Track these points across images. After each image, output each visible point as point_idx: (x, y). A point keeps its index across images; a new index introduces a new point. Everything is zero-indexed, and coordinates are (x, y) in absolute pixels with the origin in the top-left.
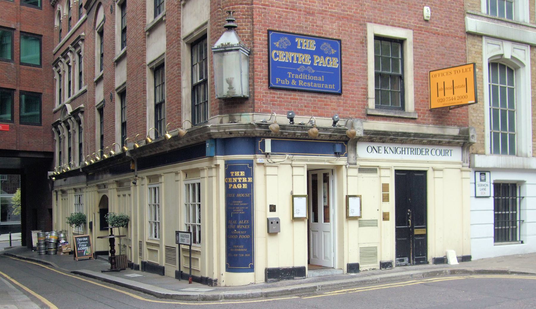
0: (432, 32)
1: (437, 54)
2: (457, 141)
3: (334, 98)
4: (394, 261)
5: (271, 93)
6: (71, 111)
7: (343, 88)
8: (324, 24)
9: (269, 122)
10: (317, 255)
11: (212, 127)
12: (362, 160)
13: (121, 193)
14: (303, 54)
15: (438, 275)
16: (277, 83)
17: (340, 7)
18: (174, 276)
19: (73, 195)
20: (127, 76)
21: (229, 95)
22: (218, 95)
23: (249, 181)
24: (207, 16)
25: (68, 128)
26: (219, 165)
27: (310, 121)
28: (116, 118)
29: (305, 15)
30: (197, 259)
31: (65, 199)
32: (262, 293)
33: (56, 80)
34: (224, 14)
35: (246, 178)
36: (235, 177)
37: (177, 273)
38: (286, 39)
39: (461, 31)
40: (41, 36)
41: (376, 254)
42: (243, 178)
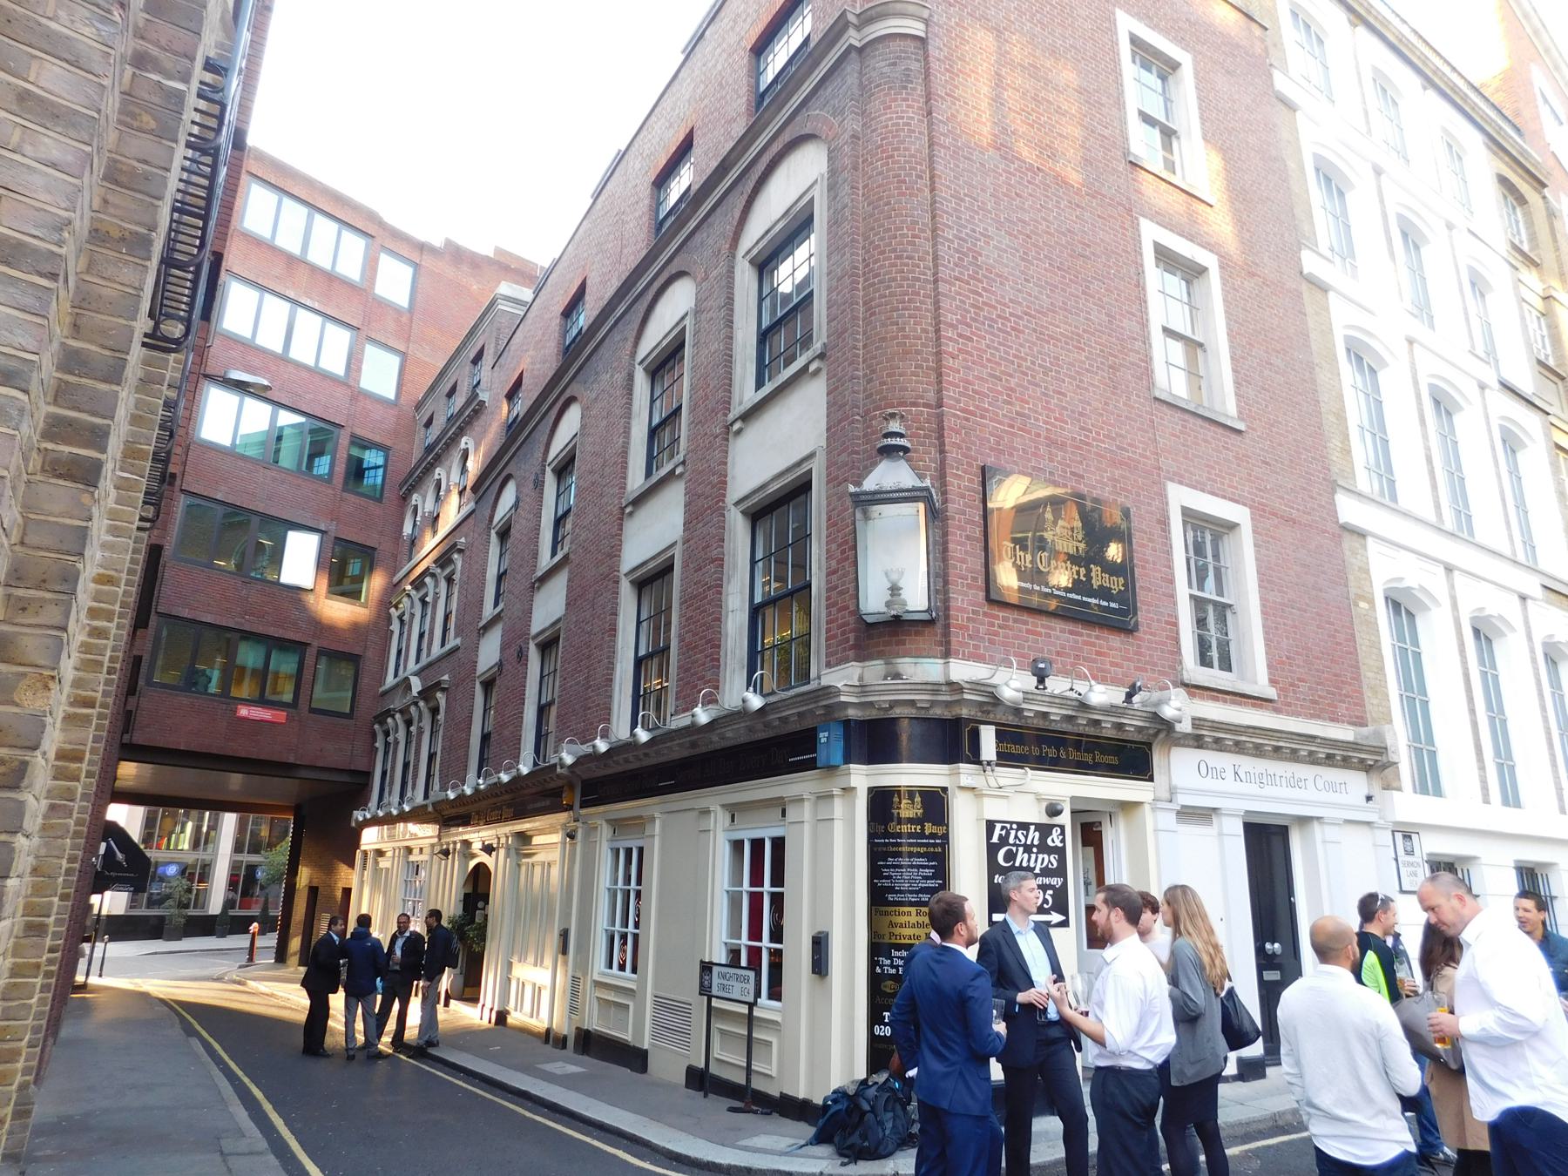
20: (568, 604)
28: (527, 695)
30: (769, 1044)
37: (691, 1071)
40: (374, 549)
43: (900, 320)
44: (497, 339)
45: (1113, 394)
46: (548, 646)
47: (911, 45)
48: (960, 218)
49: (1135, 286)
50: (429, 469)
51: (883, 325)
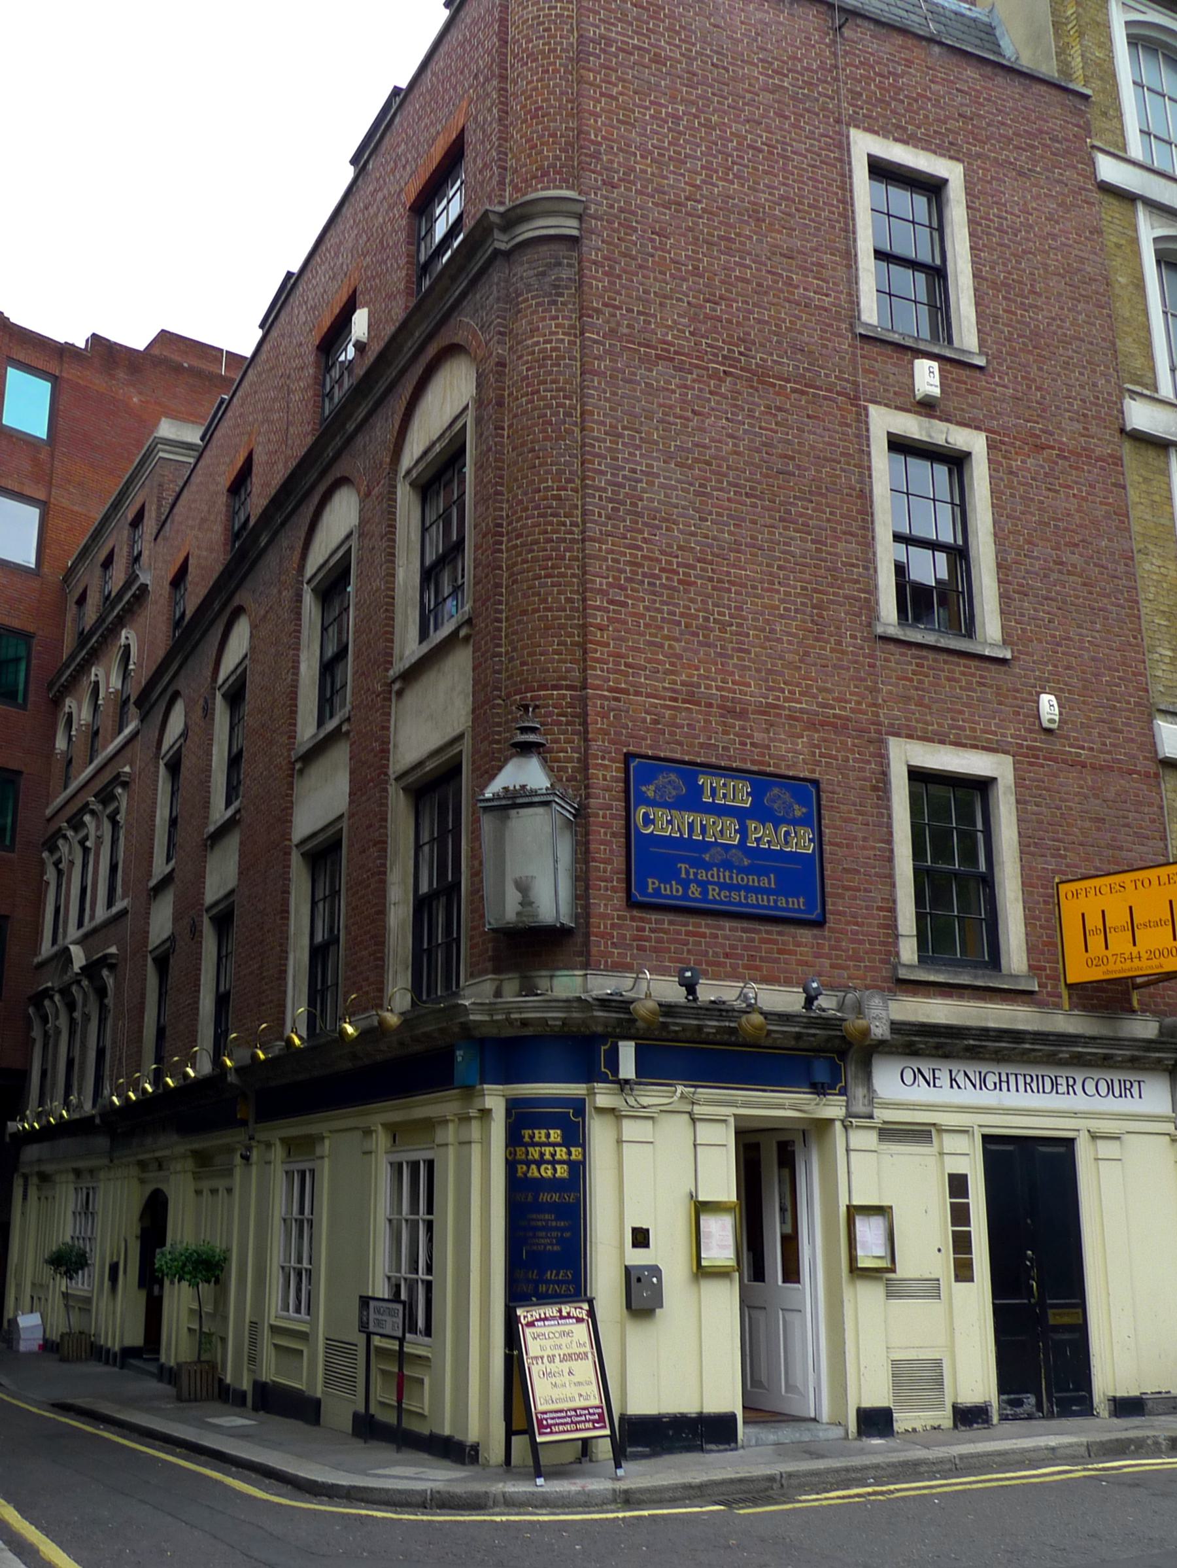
0: (1065, 762)
1: (1082, 819)
2: (1157, 1055)
3: (806, 935)
4: (995, 1404)
5: (633, 919)
6: (84, 962)
7: (829, 907)
8: (771, 740)
9: (629, 995)
10: (764, 1379)
11: (472, 1007)
12: (887, 1105)
13: (206, 1185)
14: (719, 816)
15: (1133, 1452)
16: (650, 890)
17: (815, 697)
18: (348, 1426)
19: (71, 1187)
20: (240, 873)
21: (523, 922)
22: (492, 921)
23: (573, 1157)
24: (463, 720)
25: (71, 1006)
26: (490, 1111)
27: (743, 997)
29: (722, 716)
30: (421, 1381)
31: (47, 1198)
32: (614, 1490)
33: (48, 883)
34: (511, 712)
35: (564, 1149)
36: (534, 1145)
37: (356, 1416)
38: (673, 777)
39: (1146, 758)
41: (939, 1382)
42: (558, 1149)
43: (542, 590)
44: (160, 499)
45: (817, 639)
46: (223, 920)
47: (561, 250)
48: (617, 459)
49: (859, 497)
50: (84, 668)
51: (525, 596)
